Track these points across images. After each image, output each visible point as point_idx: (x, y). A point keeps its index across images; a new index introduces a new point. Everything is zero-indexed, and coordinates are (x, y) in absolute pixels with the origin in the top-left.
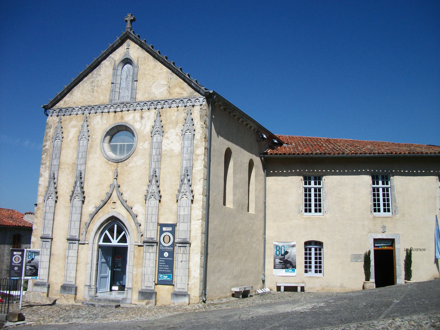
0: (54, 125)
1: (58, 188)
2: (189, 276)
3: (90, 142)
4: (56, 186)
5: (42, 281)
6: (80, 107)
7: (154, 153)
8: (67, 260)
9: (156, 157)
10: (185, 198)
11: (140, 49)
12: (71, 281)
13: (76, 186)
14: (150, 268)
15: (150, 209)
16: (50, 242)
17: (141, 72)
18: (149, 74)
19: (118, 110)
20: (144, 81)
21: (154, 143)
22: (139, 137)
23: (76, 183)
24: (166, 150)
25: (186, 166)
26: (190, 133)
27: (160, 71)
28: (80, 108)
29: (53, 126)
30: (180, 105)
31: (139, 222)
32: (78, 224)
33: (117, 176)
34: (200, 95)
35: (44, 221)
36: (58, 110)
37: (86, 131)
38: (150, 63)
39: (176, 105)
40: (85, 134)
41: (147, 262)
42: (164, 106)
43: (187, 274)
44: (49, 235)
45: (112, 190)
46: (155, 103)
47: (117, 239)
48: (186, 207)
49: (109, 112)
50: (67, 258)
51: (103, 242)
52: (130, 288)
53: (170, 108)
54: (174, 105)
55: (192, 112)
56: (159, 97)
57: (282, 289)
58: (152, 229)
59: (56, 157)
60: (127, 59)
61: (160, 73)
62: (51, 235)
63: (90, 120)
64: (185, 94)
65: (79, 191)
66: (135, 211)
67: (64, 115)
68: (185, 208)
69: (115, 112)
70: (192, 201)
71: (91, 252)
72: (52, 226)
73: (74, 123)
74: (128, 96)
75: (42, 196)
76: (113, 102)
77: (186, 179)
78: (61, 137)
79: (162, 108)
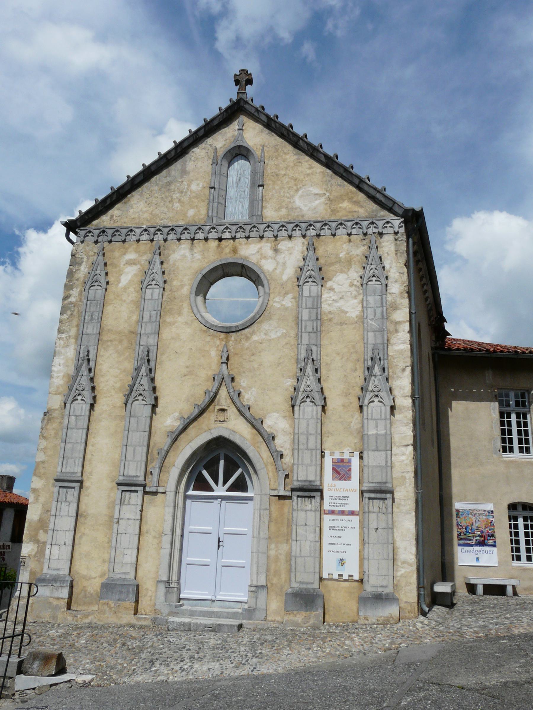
0: (88, 259)
1: (95, 380)
2: (394, 560)
3: (166, 293)
4: (92, 375)
5: (55, 573)
6: (145, 227)
7: (305, 317)
8: (115, 526)
9: (309, 324)
10: (376, 403)
11: (266, 131)
13: (138, 375)
14: (308, 543)
15: (303, 423)
16: (77, 489)
17: (269, 171)
18: (285, 175)
19: (227, 235)
20: (277, 187)
21: (304, 299)
22: (272, 286)
23: (137, 370)
24: (330, 312)
25: (374, 342)
26: (378, 283)
27: (308, 171)
28: (146, 230)
29: (85, 259)
30: (354, 231)
31: (279, 449)
32: (141, 451)
33: (228, 359)
34: (392, 215)
35: (63, 445)
36: (97, 232)
37: (160, 272)
38: (288, 157)
39: (345, 232)
40: (155, 277)
41: (301, 531)
42: (322, 233)
43: (391, 555)
44: (74, 473)
45: (216, 384)
46: (304, 226)
47: (224, 483)
48: (381, 419)
49: (206, 239)
50: (118, 522)
51: (194, 489)
52: (263, 587)
53: (334, 235)
54: (341, 231)
55: (378, 244)
56: (310, 216)
57: (480, 590)
59: (92, 319)
60: (239, 146)
61: (308, 175)
62: (80, 475)
63: (166, 252)
64: (362, 212)
65: (144, 386)
67: (110, 242)
68: (379, 421)
69: (220, 239)
70: (393, 408)
71: (171, 510)
72: (82, 456)
73: (131, 256)
74: (242, 213)
75: (59, 394)
76: (215, 222)
77: (376, 366)
78: (103, 281)
79: (318, 236)
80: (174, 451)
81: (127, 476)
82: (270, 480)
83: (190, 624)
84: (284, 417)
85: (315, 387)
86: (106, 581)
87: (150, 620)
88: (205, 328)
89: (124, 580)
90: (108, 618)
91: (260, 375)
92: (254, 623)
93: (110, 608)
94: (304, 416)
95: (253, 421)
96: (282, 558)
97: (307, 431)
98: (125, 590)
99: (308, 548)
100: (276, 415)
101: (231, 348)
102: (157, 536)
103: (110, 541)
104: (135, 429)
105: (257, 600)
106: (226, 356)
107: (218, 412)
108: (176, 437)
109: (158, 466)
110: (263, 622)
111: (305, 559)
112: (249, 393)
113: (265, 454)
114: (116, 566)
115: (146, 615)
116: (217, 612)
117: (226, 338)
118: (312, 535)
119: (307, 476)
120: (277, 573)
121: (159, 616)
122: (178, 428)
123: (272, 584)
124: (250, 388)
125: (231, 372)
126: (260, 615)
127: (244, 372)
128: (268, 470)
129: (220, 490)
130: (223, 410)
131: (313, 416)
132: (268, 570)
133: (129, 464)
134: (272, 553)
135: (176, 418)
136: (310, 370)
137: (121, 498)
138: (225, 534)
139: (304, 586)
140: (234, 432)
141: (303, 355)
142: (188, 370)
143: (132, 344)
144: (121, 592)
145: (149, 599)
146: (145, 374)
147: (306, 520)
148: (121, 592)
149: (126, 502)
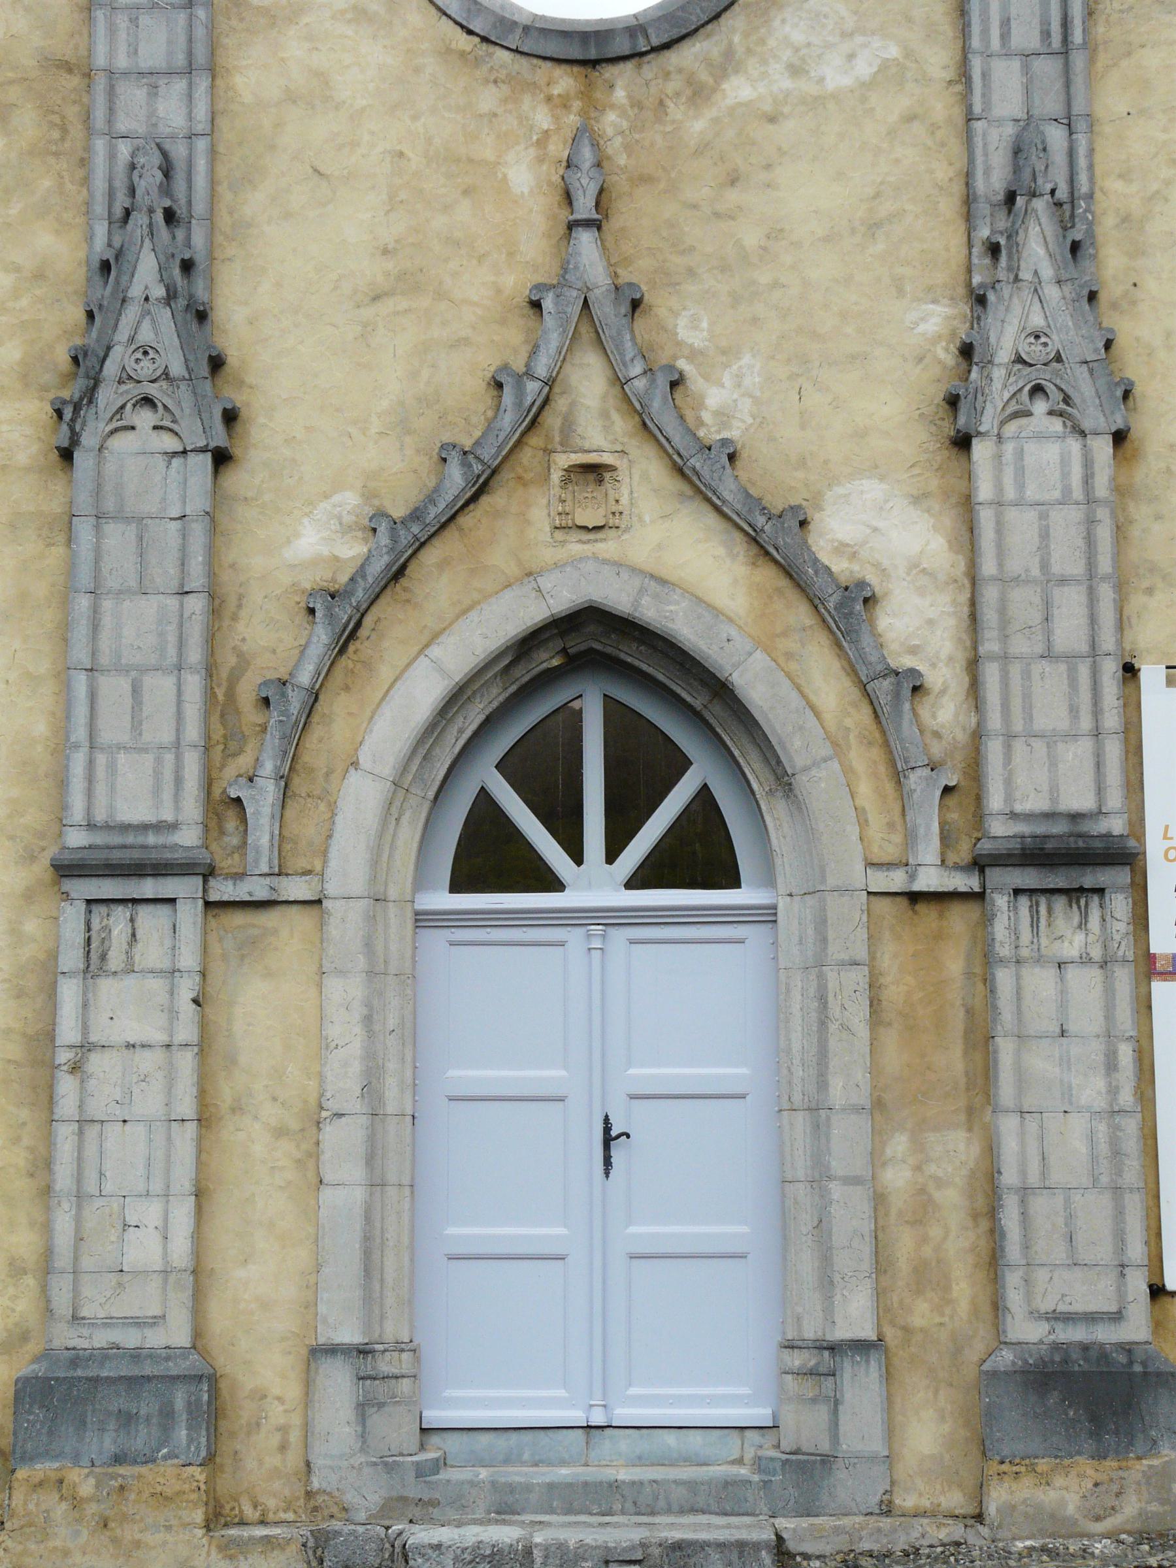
8: (67, 1085)
12: (130, 1303)
41: (1042, 1062)
51: (456, 886)
52: (861, 1347)
58: (1064, 725)
66: (841, 548)
80: (347, 688)
81: (108, 827)
82: (862, 821)
83: (528, 1552)
84: (917, 499)
85: (1072, 337)
86: (40, 1369)
87: (294, 1548)
88: (464, 42)
89: (136, 1355)
90: (66, 1553)
91: (776, 285)
92: (837, 1530)
93: (76, 1503)
94: (1021, 486)
95: (760, 521)
96: (952, 1199)
97: (1045, 565)
98: (147, 1406)
99: (1082, 1148)
100: (872, 489)
101: (614, 147)
102: (294, 1125)
103: (43, 1164)
104: (133, 583)
105: (835, 1411)
106: (592, 190)
107: (566, 481)
108: (348, 617)
109: (268, 767)
110: (886, 1523)
111: (1067, 1201)
112: (727, 379)
113: (829, 686)
114: (87, 1291)
115: (263, 1522)
116: (637, 1485)
117: (586, 94)
118: (1099, 1083)
119: (1054, 790)
120: (930, 1277)
121: (336, 1525)
122: (361, 571)
123: (906, 1330)
124: (729, 353)
125: (625, 276)
126: (853, 1488)
127: (691, 272)
128: (848, 770)
129: (595, 883)
130: (594, 472)
131: (1067, 490)
132: (881, 1264)
133: (112, 767)
134: (897, 1179)
135: (348, 519)
136: (1041, 251)
137: (88, 941)
138: (633, 1097)
139: (1076, 1334)
140: (663, 582)
141: (994, 178)
142: (389, 265)
143: (64, 130)
144: (127, 1420)
145: (275, 1440)
146: (159, 292)
147: (1063, 1004)
148: (127, 1420)
149: (116, 960)
